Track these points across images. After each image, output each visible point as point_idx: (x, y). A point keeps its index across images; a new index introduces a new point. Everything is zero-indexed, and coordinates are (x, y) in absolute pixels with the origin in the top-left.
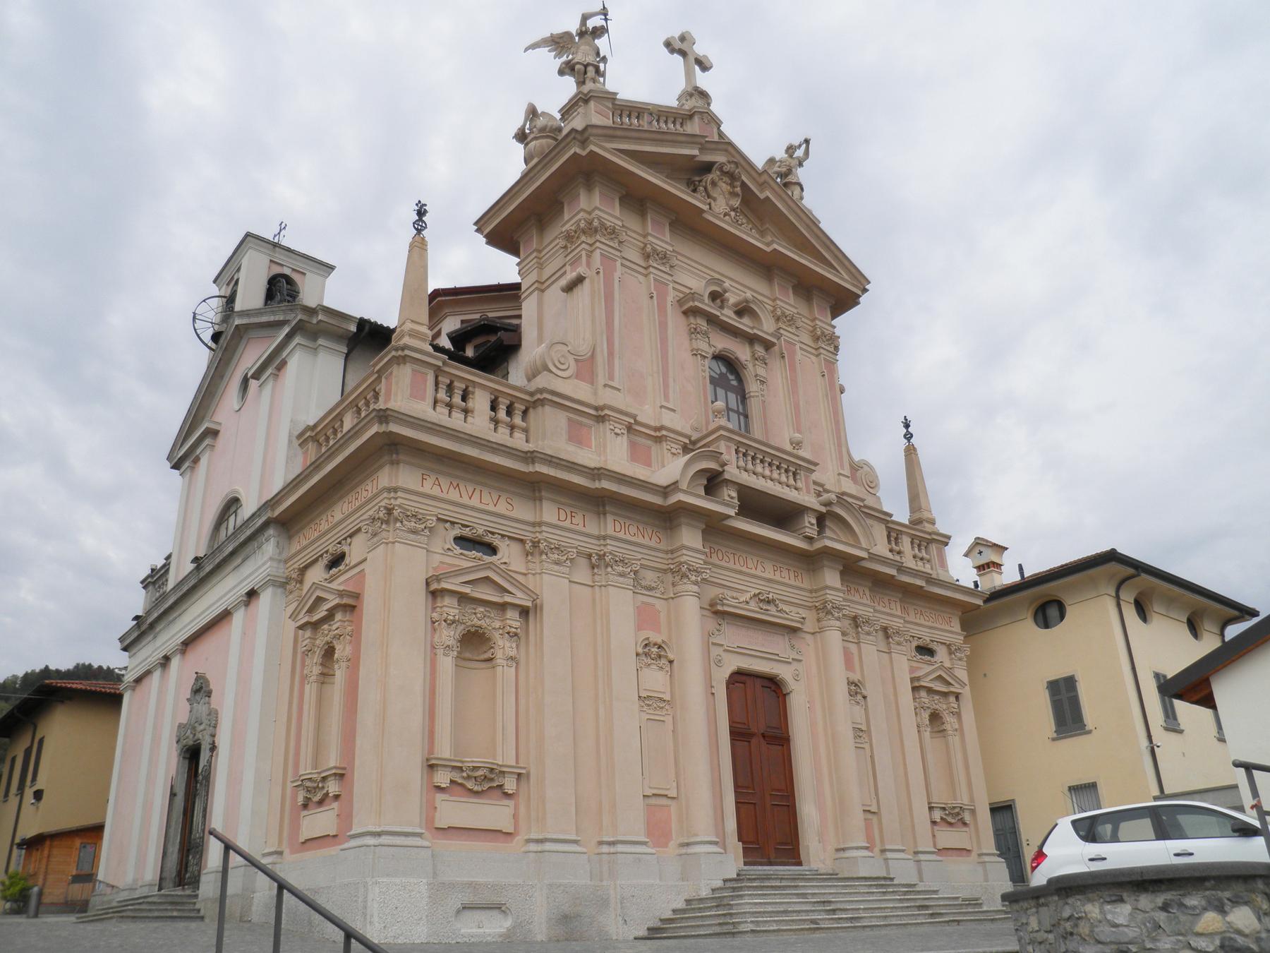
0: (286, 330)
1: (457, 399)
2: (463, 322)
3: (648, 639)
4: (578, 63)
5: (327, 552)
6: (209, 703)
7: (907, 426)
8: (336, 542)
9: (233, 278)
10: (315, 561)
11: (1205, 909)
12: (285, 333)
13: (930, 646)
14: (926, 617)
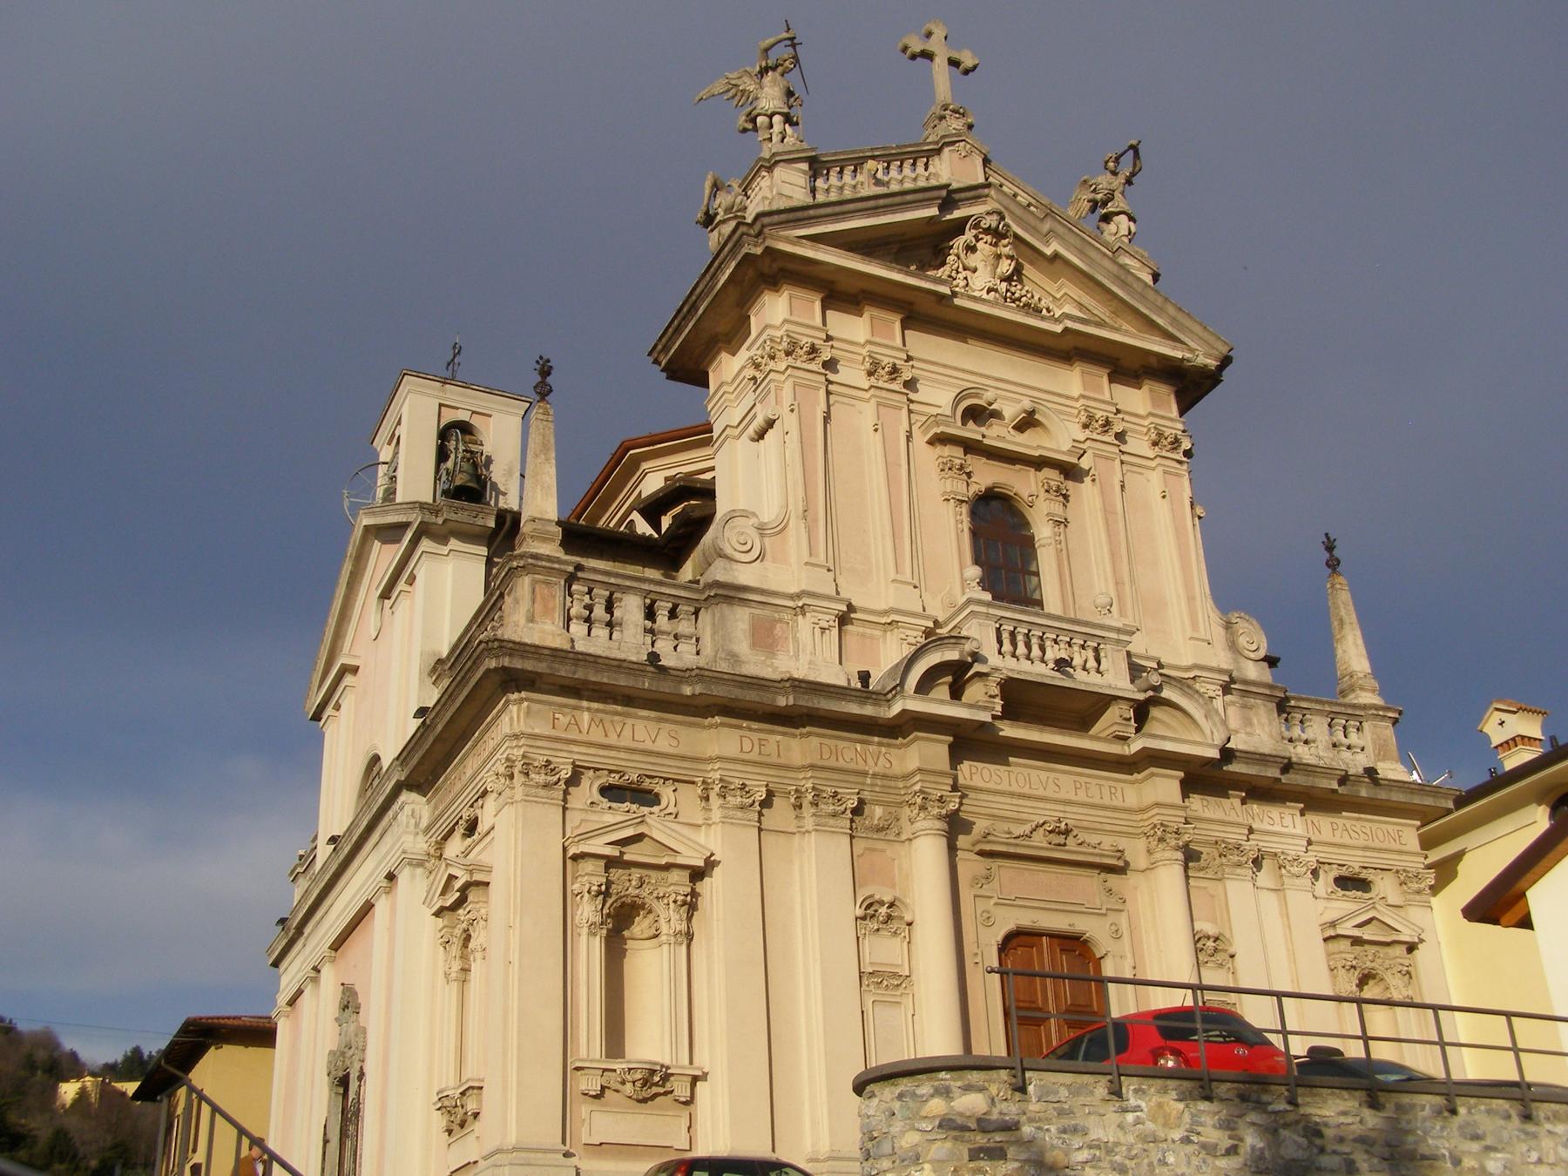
0: (409, 535)
1: (599, 611)
2: (666, 479)
3: (871, 896)
4: (759, 115)
5: (461, 818)
6: (357, 1021)
7: (1330, 547)
8: (469, 804)
10: (452, 831)
11: (932, 1096)
12: (408, 539)
13: (1362, 876)
14: (1353, 834)
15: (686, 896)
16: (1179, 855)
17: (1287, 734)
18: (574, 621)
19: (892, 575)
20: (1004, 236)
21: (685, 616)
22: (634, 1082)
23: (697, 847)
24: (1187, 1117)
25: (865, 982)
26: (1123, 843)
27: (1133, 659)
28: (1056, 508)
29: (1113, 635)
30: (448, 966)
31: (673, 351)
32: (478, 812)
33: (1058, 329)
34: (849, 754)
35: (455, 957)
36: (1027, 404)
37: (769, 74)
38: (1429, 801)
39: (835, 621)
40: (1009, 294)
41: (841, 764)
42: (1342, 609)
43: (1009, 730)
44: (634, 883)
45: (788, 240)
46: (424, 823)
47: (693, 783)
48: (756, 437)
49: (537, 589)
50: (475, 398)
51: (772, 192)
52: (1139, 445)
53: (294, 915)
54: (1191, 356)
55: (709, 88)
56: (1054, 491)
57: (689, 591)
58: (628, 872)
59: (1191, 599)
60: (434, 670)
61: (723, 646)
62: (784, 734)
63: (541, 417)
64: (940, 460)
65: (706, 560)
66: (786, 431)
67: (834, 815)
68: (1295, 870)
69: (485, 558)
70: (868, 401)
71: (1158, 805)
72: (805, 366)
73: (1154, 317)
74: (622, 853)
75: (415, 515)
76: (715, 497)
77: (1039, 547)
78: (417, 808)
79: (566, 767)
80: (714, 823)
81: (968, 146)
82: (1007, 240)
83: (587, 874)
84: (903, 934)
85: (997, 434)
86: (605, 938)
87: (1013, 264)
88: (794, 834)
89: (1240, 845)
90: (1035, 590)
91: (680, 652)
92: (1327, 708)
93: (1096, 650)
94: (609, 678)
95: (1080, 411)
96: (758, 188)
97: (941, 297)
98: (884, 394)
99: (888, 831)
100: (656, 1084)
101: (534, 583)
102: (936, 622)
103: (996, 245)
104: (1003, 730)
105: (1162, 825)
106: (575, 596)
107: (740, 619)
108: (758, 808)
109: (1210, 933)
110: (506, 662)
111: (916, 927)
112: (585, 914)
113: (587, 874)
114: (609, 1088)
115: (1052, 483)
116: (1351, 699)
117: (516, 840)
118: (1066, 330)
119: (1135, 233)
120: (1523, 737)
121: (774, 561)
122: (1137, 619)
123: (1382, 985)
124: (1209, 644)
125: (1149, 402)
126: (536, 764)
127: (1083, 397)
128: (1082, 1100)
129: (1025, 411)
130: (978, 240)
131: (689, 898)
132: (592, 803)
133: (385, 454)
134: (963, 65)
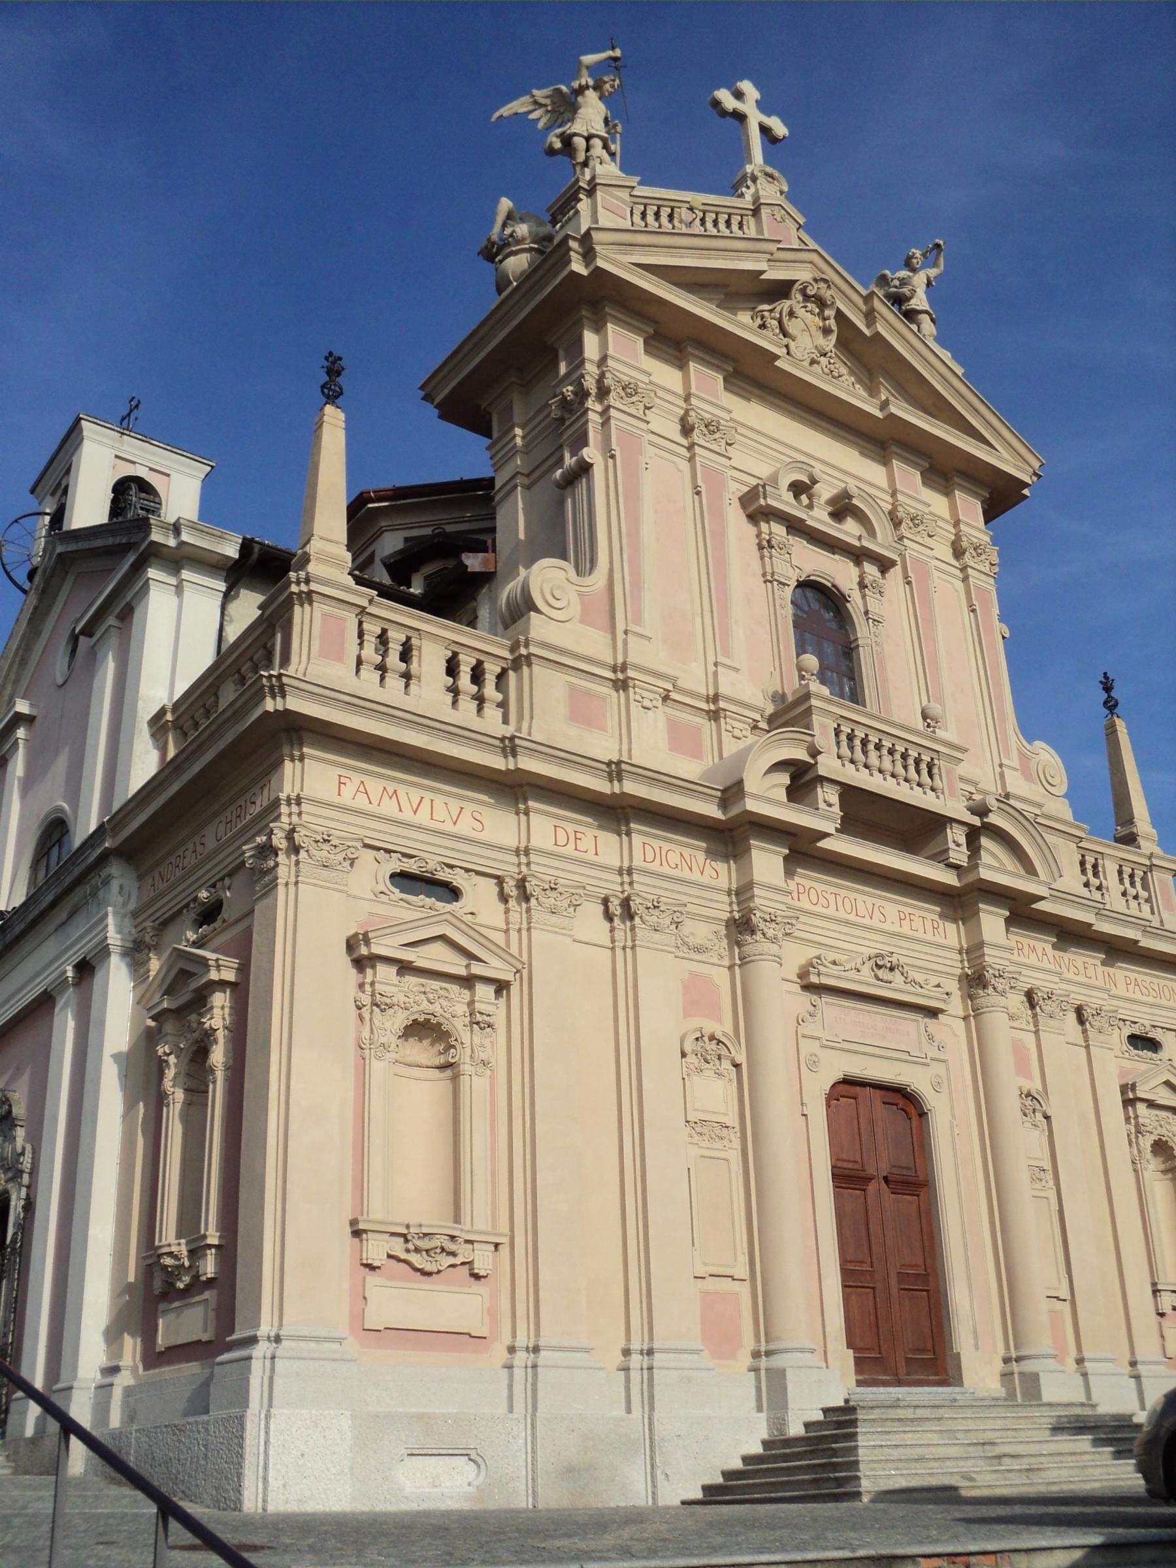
1: (393, 659)
2: (406, 540)
7: (1108, 687)
9: (59, 484)
10: (179, 913)
13: (1150, 1035)
69: (222, 595)
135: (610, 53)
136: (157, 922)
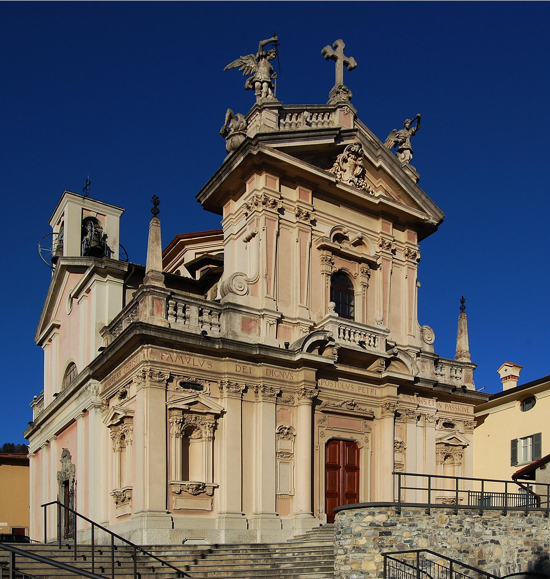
0: (88, 272)
1: (180, 312)
4: (257, 81)
5: (119, 391)
7: (462, 302)
8: (123, 386)
9: (60, 220)
10: (114, 395)
15: (213, 424)
16: (393, 414)
17: (435, 372)
18: (170, 316)
19: (299, 304)
20: (360, 156)
21: (215, 316)
22: (192, 489)
23: (218, 406)
24: (448, 520)
25: (277, 455)
26: (374, 409)
27: (387, 343)
28: (365, 280)
29: (382, 333)
30: (114, 446)
31: (208, 197)
32: (128, 390)
33: (377, 202)
34: (277, 373)
35: (117, 443)
36: (360, 234)
37: (263, 60)
38: (478, 398)
39: (275, 321)
40: (358, 184)
41: (274, 377)
42: (463, 326)
43: (340, 368)
44: (193, 419)
45: (269, 149)
46: (100, 392)
47: (216, 382)
48: (246, 241)
49: (154, 302)
50: (98, 207)
51: (261, 123)
52: (400, 255)
53: (36, 421)
54: (428, 218)
55: (232, 63)
56: (365, 273)
57: (217, 306)
58: (191, 415)
59: (410, 319)
60: (102, 331)
61: (230, 329)
62: (253, 365)
63: (155, 224)
64: (322, 256)
65: (224, 293)
66: (260, 239)
67: (271, 396)
68: (431, 420)
70: (295, 228)
71: (389, 396)
72: (270, 210)
73: (416, 200)
74: (189, 408)
75: (92, 263)
76: (224, 265)
77: (356, 295)
78: (97, 385)
79: (167, 374)
80: (224, 398)
81: (348, 109)
82: (361, 158)
83: (175, 415)
84: (292, 439)
85: (346, 247)
86: (182, 439)
87: (361, 170)
88: (254, 402)
89: (414, 411)
90: (352, 312)
91: (213, 331)
92: (451, 363)
93: (374, 338)
94: (186, 340)
95: (379, 239)
96: (254, 120)
97: (331, 182)
98: (302, 225)
99: (290, 402)
100: (201, 489)
101: (153, 298)
102: (314, 324)
103: (356, 160)
104: (337, 368)
105: (389, 404)
106: (170, 305)
107: (238, 319)
108: (242, 393)
109: (399, 441)
110: (144, 332)
111: (298, 437)
112: (174, 430)
113: (175, 415)
114: (183, 491)
115: (365, 269)
116: (460, 360)
117: (147, 402)
118: (380, 202)
119: (412, 159)
120: (512, 376)
121: (252, 295)
122: (275, 295)
123: (452, 459)
124: (414, 337)
125: (407, 239)
126: (155, 373)
127: (381, 233)
128: (417, 516)
129: (359, 238)
130: (349, 156)
131: (214, 425)
132: (177, 389)
133: (56, 229)
134: (350, 65)
135: (273, 39)
136: (107, 398)
